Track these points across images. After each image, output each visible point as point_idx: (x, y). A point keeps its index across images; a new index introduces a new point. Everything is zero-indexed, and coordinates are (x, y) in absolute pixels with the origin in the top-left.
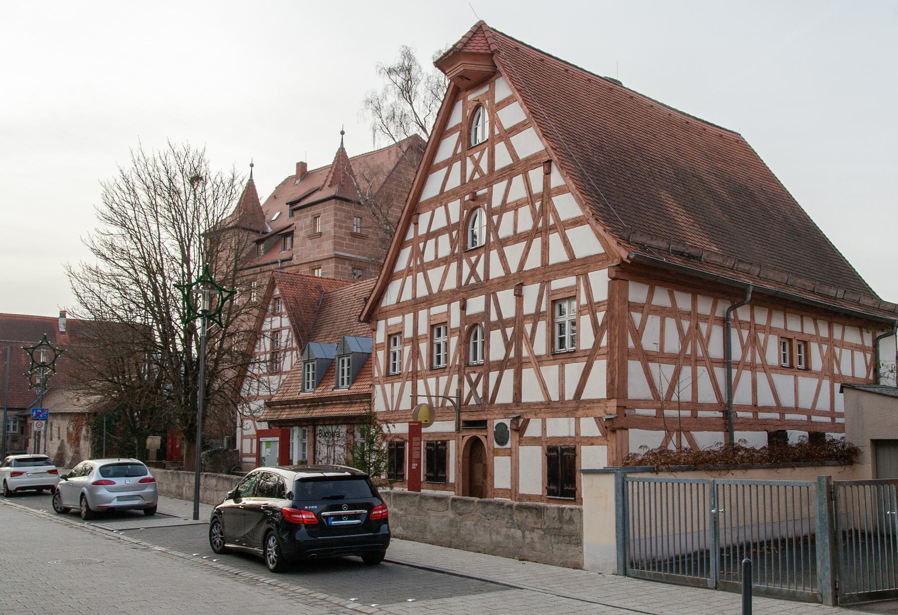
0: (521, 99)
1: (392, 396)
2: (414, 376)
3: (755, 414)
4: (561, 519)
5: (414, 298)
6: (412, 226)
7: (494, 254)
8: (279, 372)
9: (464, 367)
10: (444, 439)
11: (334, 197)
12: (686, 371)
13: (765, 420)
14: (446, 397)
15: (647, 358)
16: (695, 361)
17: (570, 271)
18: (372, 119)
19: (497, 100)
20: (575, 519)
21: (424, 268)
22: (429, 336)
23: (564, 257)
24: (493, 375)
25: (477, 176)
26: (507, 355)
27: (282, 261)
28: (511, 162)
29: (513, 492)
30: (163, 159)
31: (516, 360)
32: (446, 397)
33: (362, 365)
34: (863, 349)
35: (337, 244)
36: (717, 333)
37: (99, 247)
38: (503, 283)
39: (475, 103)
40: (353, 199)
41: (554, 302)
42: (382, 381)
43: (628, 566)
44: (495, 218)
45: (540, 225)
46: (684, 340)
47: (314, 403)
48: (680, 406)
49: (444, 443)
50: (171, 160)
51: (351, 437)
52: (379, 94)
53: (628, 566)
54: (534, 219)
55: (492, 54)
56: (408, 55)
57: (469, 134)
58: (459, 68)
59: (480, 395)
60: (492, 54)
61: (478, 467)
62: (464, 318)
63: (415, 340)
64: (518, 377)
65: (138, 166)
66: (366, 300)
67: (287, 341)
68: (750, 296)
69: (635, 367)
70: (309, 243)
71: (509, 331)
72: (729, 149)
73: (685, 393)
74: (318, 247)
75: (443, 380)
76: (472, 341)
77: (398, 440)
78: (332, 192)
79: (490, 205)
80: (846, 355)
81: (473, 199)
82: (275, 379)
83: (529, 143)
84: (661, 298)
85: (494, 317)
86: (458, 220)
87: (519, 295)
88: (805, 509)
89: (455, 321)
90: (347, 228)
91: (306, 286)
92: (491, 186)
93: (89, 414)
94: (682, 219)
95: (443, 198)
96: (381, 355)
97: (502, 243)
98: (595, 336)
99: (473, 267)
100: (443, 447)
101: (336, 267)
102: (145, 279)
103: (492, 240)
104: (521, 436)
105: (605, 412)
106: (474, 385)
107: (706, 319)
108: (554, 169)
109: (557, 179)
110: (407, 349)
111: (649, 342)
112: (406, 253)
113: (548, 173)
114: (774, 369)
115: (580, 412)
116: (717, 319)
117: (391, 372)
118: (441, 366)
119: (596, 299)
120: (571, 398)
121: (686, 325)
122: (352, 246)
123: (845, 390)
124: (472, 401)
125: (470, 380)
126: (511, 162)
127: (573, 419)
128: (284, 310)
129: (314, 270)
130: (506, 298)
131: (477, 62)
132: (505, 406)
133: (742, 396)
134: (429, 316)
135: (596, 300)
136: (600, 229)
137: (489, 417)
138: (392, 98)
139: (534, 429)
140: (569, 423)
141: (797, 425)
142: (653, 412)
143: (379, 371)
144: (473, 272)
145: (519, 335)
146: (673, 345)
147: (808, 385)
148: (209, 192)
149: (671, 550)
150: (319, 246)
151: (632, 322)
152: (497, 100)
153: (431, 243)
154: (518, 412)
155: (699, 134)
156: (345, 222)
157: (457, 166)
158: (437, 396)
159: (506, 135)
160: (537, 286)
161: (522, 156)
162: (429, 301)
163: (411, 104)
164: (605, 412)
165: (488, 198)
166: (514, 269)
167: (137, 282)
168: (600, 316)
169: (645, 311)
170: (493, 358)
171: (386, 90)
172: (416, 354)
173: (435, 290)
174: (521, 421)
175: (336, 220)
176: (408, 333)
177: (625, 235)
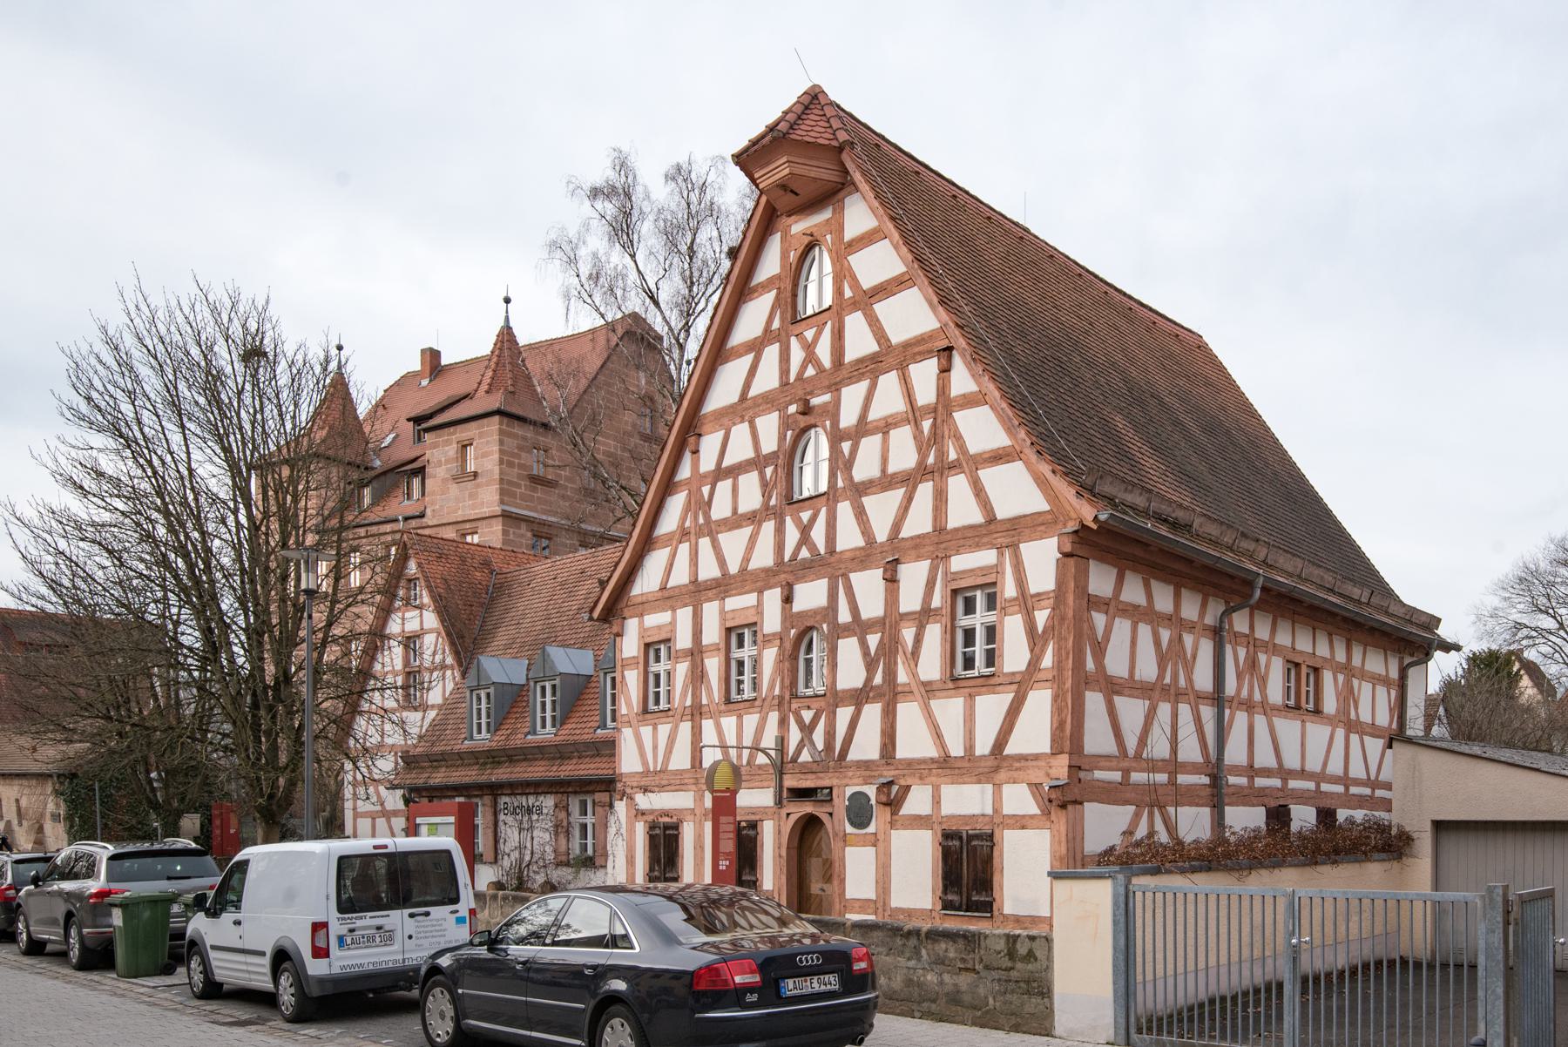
0: (896, 235)
1: (655, 747)
2: (696, 713)
3: (1251, 779)
4: (1011, 954)
5: (694, 581)
6: (687, 458)
7: (844, 509)
8: (424, 707)
9: (789, 698)
10: (753, 818)
11: (499, 412)
12: (1164, 709)
13: (1264, 789)
14: (756, 748)
15: (1112, 688)
16: (1175, 695)
17: (985, 540)
18: (558, 277)
19: (849, 235)
20: (1038, 954)
21: (712, 530)
22: (722, 646)
23: (977, 517)
24: (844, 715)
25: (810, 371)
26: (869, 679)
27: (406, 519)
28: (875, 348)
29: (880, 905)
30: (187, 310)
31: (886, 687)
32: (756, 748)
33: (578, 694)
34: (1385, 681)
35: (505, 493)
36: (1206, 649)
37: (69, 469)
38: (862, 559)
39: (807, 240)
40: (531, 416)
41: (955, 592)
42: (634, 722)
43: (1133, 1030)
44: (846, 446)
45: (931, 460)
46: (1162, 661)
47: (492, 757)
48: (1153, 766)
49: (676, 827)
50: (204, 314)
51: (563, 815)
52: (572, 233)
53: (1133, 1030)
54: (919, 450)
55: (840, 149)
56: (622, 165)
57: (795, 296)
58: (780, 169)
59: (820, 746)
60: (840, 149)
61: (815, 865)
62: (788, 617)
63: (696, 653)
64: (889, 716)
65: (137, 321)
66: (603, 584)
67: (434, 653)
68: (1258, 593)
69: (1094, 701)
70: (454, 489)
71: (873, 640)
72: (1188, 356)
73: (1159, 747)
74: (471, 496)
75: (751, 721)
76: (802, 656)
77: (667, 820)
78: (495, 401)
79: (835, 423)
80: (1364, 690)
81: (803, 410)
82: (413, 717)
83: (912, 315)
84: (1133, 592)
85: (844, 616)
86: (775, 448)
87: (891, 580)
88: (1342, 929)
89: (772, 622)
90: (521, 466)
91: (463, 560)
92: (838, 390)
93: (59, 776)
94: (1150, 464)
95: (746, 408)
96: (632, 678)
97: (859, 490)
98: (1032, 651)
99: (805, 531)
100: (752, 833)
101: (505, 532)
102: (161, 531)
103: (840, 484)
104: (894, 813)
105: (1048, 775)
106: (807, 730)
107: (1191, 627)
108: (957, 360)
109: (962, 380)
110: (682, 669)
111: (1116, 664)
112: (676, 504)
113: (945, 370)
114: (1275, 708)
115: (1002, 775)
116: (1206, 628)
117: (652, 707)
118: (746, 697)
119: (1033, 589)
120: (987, 751)
121: (1165, 635)
122: (531, 499)
123: (1395, 744)
124: (805, 756)
125: (800, 721)
126: (875, 348)
127: (989, 788)
128: (426, 600)
129: (464, 535)
130: (868, 587)
131: (813, 158)
132: (866, 765)
133: (1235, 753)
134: (722, 612)
135: (1033, 589)
136: (1045, 469)
137: (835, 782)
138: (597, 242)
139: (918, 801)
140: (983, 792)
141: (1303, 798)
142: (1116, 776)
143: (629, 704)
144: (805, 538)
145: (891, 647)
146: (1147, 669)
147: (1318, 733)
148: (284, 380)
149: (1170, 997)
150: (472, 496)
151: (1092, 628)
152: (849, 235)
153: (724, 487)
154: (888, 774)
155: (1148, 330)
156: (519, 457)
157: (772, 353)
158: (740, 748)
159: (867, 299)
160: (925, 565)
161: (896, 338)
162: (723, 586)
163: (633, 256)
164: (1048, 775)
165: (833, 411)
166: (881, 535)
167: (148, 537)
168: (1041, 617)
169: (1111, 610)
170: (842, 684)
171: (586, 226)
172: (698, 676)
173: (733, 568)
174: (895, 788)
175: (501, 452)
176: (683, 641)
177: (1089, 482)
